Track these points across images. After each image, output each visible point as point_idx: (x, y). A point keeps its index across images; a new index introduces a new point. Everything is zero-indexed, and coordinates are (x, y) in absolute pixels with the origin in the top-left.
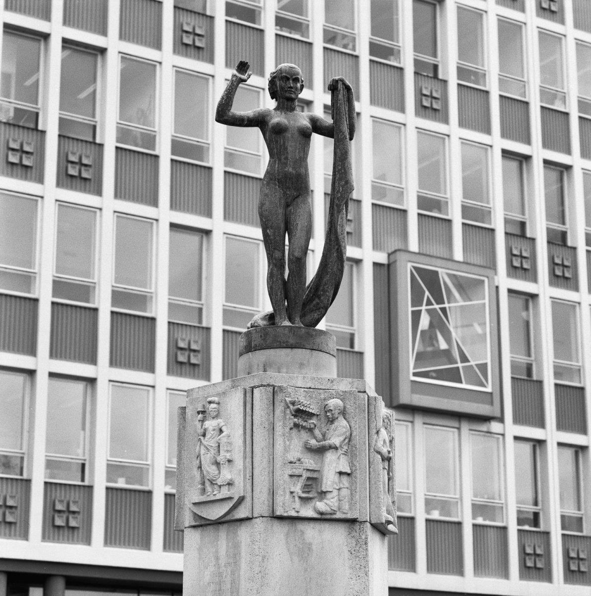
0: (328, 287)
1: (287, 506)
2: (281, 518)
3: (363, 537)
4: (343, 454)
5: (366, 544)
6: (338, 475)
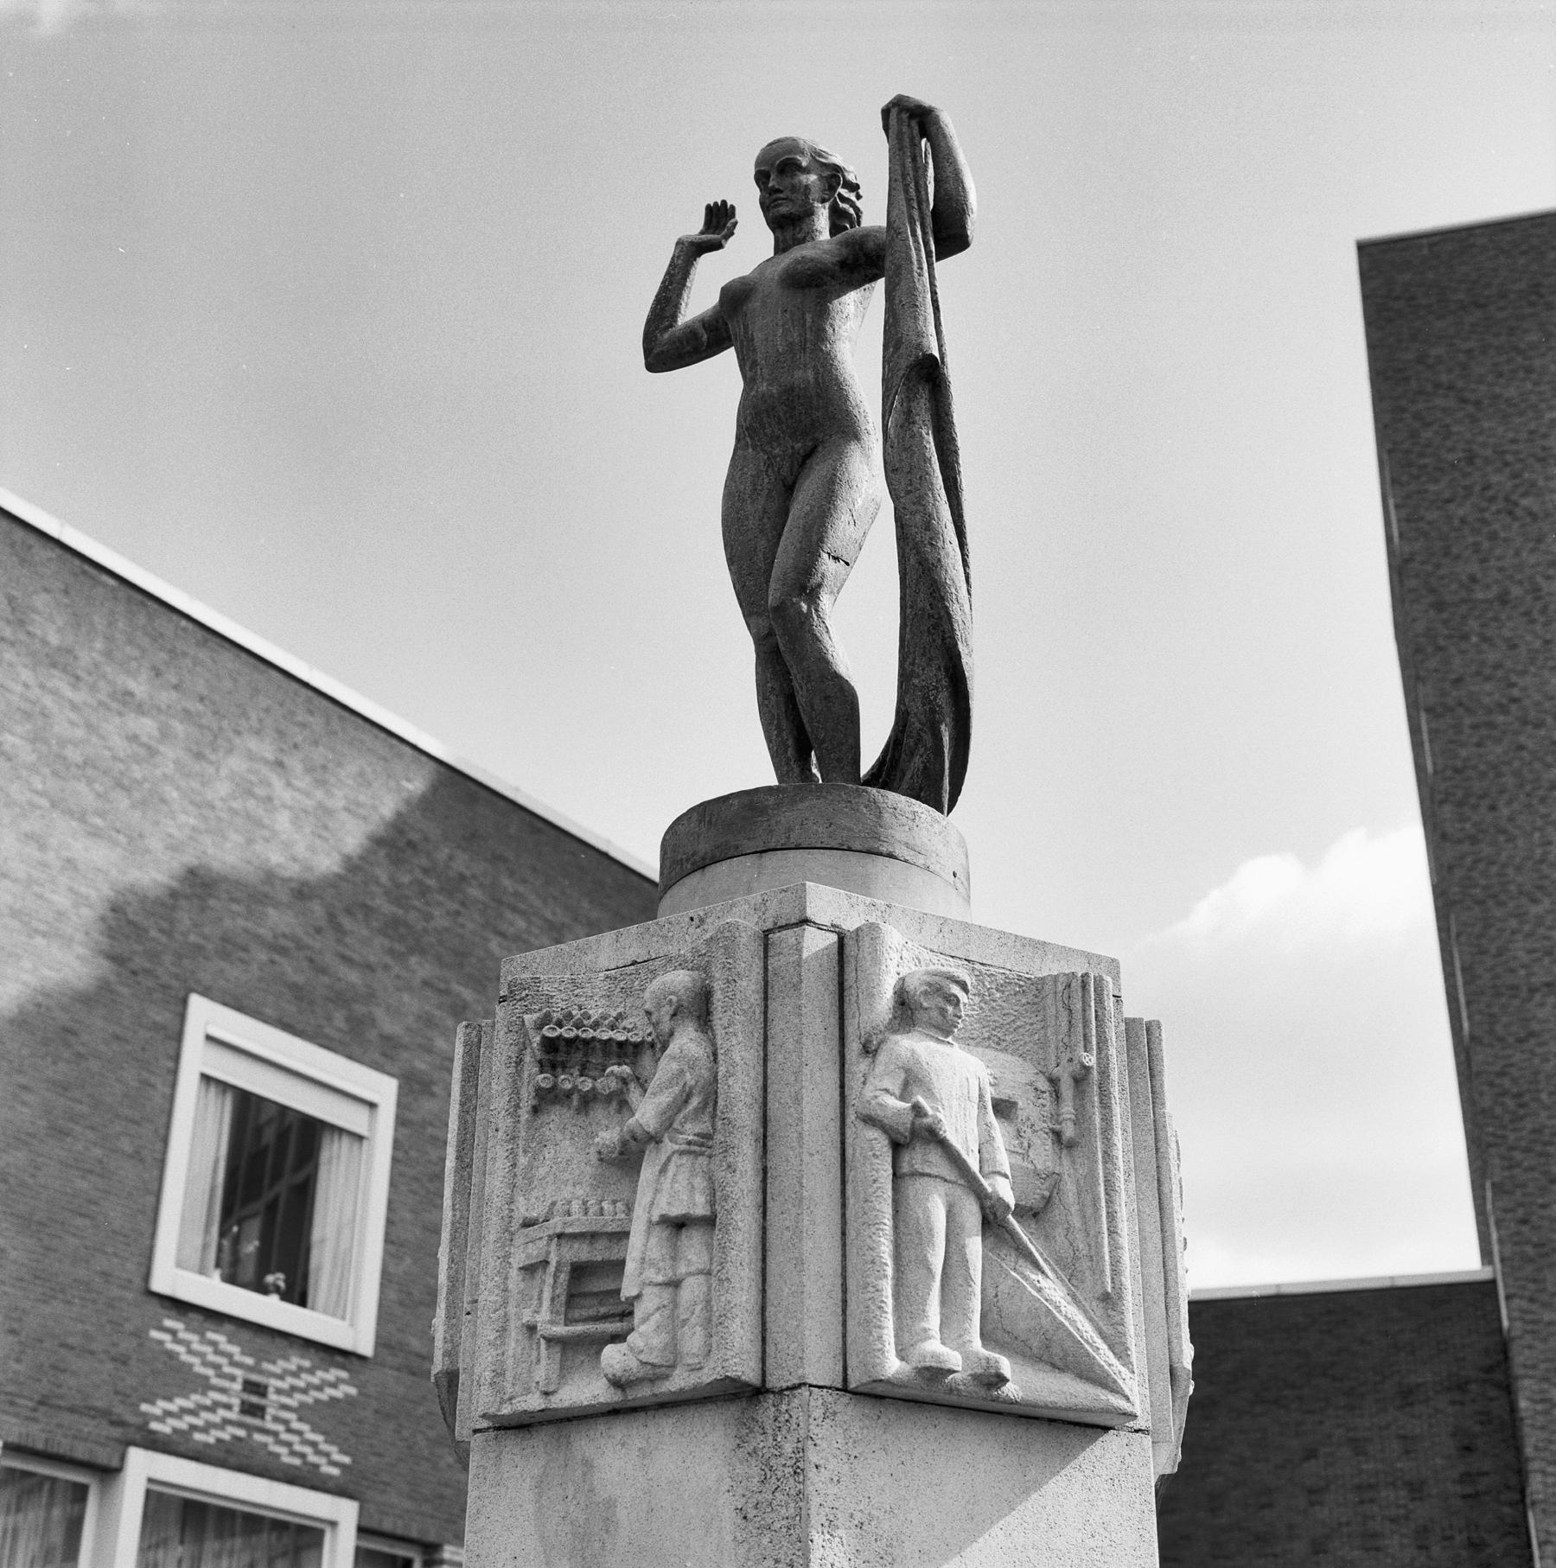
0: (913, 664)
1: (535, 1384)
2: (854, 1393)
3: (788, 1448)
4: (682, 1153)
5: (797, 1472)
6: (661, 1234)
